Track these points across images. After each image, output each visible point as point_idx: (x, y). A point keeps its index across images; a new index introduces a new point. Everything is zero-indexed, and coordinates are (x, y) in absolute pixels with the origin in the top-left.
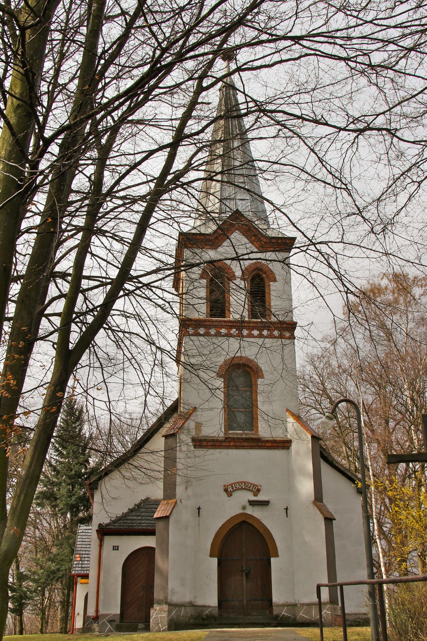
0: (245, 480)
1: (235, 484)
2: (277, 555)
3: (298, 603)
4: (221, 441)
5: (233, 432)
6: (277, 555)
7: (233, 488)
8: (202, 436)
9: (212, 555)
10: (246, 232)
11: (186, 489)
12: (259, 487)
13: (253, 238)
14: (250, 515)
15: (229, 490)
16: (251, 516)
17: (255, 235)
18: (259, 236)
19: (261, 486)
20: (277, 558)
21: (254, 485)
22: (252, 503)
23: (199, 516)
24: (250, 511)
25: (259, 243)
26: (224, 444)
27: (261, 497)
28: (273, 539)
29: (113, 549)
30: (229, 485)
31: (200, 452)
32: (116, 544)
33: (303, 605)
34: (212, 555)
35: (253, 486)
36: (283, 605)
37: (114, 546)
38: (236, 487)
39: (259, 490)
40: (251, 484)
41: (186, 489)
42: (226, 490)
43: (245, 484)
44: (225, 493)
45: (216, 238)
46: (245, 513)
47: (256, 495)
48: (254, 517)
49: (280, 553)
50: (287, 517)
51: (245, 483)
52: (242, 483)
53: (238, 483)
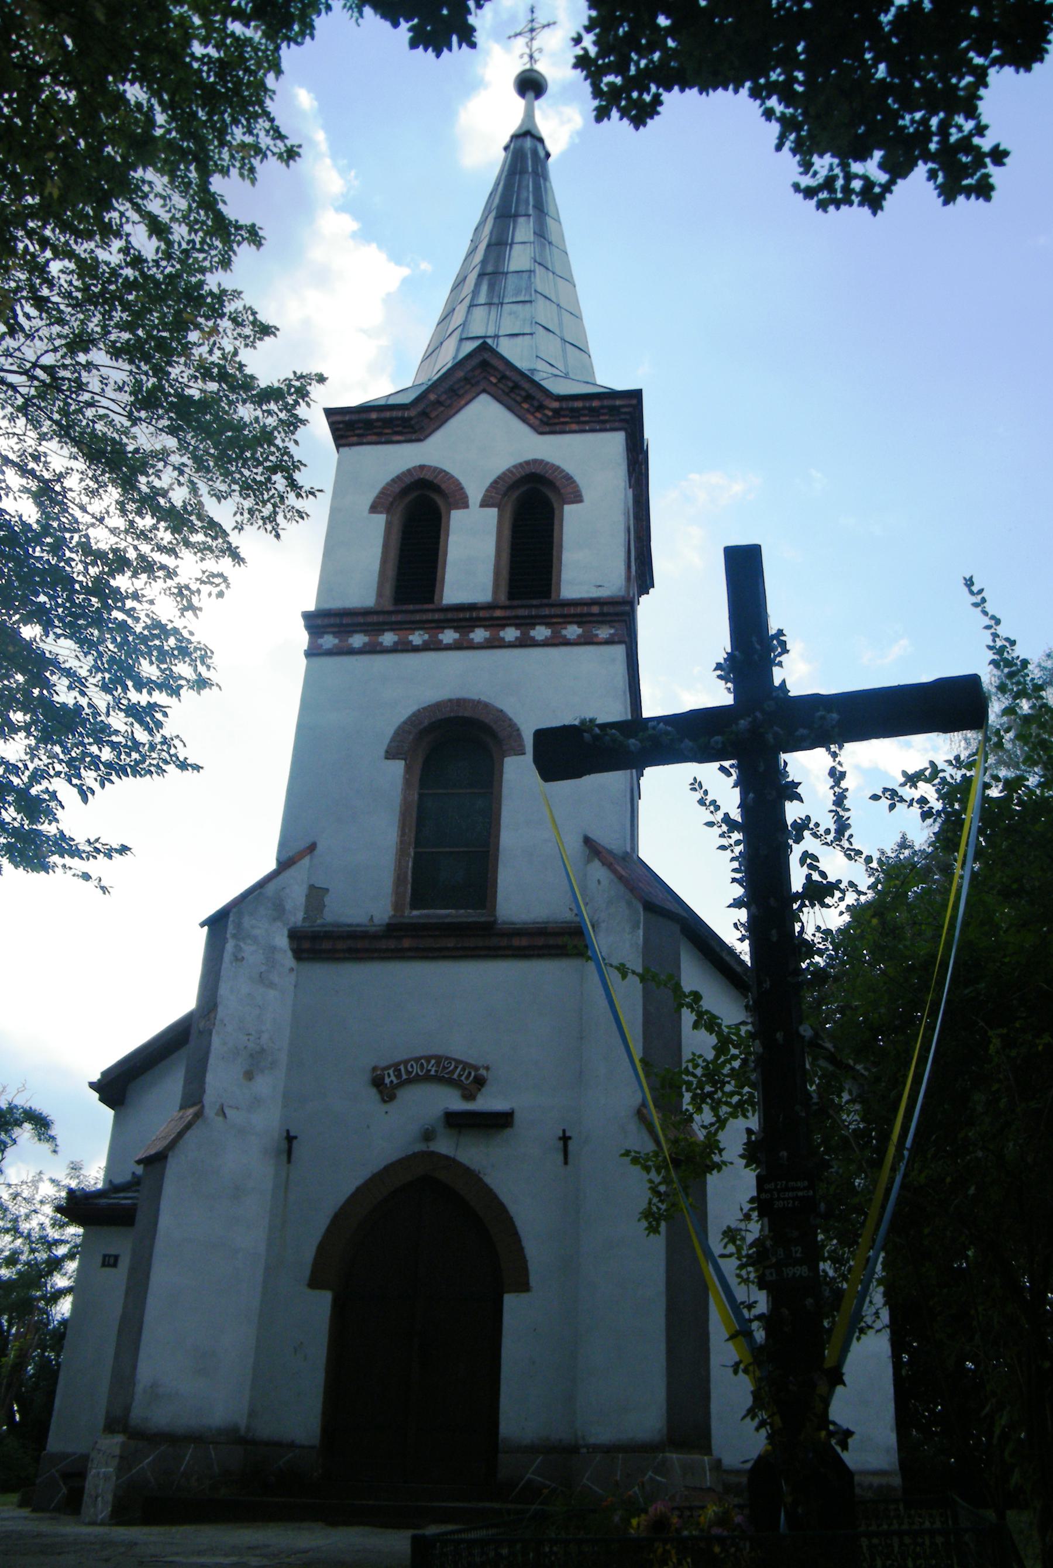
0: (440, 1052)
1: (406, 1062)
2: (524, 1286)
3: (581, 1442)
4: (375, 937)
5: (426, 911)
6: (524, 1286)
7: (399, 1076)
8: (323, 925)
9: (315, 1283)
10: (507, 394)
11: (249, 1076)
12: (483, 1072)
13: (525, 406)
14: (447, 1158)
15: (387, 1081)
16: (450, 1162)
17: (529, 398)
18: (539, 395)
19: (487, 1068)
20: (523, 1296)
21: (466, 1065)
22: (456, 1121)
23: (289, 1161)
24: (443, 1146)
25: (538, 415)
26: (383, 944)
27: (487, 1102)
28: (516, 1233)
29: (104, 1265)
30: (388, 1068)
31: (322, 972)
32: (113, 1251)
33: (596, 1448)
34: (315, 1283)
35: (464, 1069)
36: (532, 1449)
37: (105, 1256)
38: (408, 1073)
39: (480, 1082)
40: (458, 1062)
41: (249, 1076)
42: (377, 1082)
43: (438, 1064)
44: (373, 1091)
45: (424, 414)
46: (433, 1154)
47: (469, 1096)
48: (460, 1165)
49: (533, 1280)
50: (566, 1163)
51: (439, 1059)
52: (428, 1059)
53: (417, 1060)
